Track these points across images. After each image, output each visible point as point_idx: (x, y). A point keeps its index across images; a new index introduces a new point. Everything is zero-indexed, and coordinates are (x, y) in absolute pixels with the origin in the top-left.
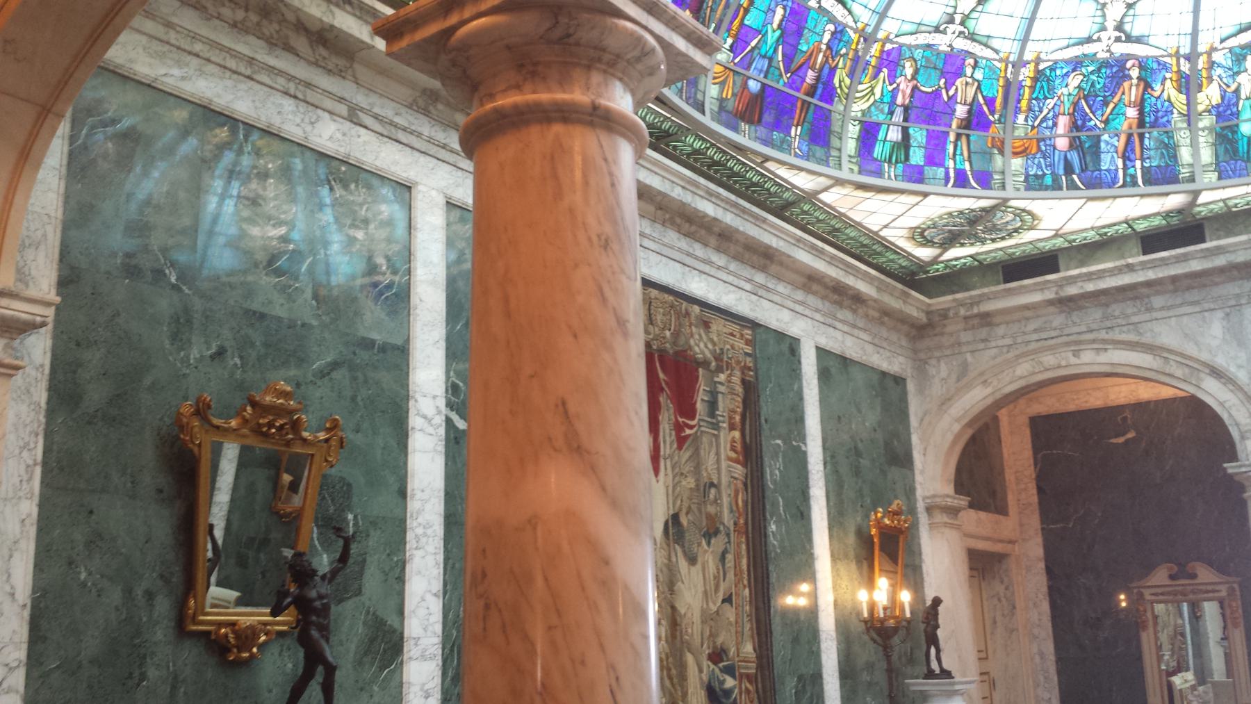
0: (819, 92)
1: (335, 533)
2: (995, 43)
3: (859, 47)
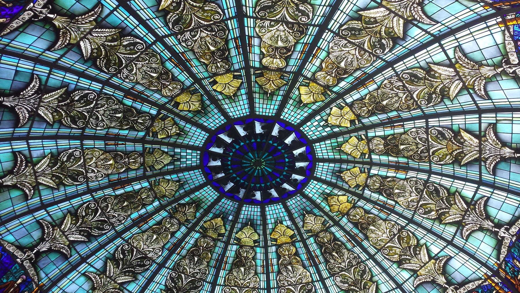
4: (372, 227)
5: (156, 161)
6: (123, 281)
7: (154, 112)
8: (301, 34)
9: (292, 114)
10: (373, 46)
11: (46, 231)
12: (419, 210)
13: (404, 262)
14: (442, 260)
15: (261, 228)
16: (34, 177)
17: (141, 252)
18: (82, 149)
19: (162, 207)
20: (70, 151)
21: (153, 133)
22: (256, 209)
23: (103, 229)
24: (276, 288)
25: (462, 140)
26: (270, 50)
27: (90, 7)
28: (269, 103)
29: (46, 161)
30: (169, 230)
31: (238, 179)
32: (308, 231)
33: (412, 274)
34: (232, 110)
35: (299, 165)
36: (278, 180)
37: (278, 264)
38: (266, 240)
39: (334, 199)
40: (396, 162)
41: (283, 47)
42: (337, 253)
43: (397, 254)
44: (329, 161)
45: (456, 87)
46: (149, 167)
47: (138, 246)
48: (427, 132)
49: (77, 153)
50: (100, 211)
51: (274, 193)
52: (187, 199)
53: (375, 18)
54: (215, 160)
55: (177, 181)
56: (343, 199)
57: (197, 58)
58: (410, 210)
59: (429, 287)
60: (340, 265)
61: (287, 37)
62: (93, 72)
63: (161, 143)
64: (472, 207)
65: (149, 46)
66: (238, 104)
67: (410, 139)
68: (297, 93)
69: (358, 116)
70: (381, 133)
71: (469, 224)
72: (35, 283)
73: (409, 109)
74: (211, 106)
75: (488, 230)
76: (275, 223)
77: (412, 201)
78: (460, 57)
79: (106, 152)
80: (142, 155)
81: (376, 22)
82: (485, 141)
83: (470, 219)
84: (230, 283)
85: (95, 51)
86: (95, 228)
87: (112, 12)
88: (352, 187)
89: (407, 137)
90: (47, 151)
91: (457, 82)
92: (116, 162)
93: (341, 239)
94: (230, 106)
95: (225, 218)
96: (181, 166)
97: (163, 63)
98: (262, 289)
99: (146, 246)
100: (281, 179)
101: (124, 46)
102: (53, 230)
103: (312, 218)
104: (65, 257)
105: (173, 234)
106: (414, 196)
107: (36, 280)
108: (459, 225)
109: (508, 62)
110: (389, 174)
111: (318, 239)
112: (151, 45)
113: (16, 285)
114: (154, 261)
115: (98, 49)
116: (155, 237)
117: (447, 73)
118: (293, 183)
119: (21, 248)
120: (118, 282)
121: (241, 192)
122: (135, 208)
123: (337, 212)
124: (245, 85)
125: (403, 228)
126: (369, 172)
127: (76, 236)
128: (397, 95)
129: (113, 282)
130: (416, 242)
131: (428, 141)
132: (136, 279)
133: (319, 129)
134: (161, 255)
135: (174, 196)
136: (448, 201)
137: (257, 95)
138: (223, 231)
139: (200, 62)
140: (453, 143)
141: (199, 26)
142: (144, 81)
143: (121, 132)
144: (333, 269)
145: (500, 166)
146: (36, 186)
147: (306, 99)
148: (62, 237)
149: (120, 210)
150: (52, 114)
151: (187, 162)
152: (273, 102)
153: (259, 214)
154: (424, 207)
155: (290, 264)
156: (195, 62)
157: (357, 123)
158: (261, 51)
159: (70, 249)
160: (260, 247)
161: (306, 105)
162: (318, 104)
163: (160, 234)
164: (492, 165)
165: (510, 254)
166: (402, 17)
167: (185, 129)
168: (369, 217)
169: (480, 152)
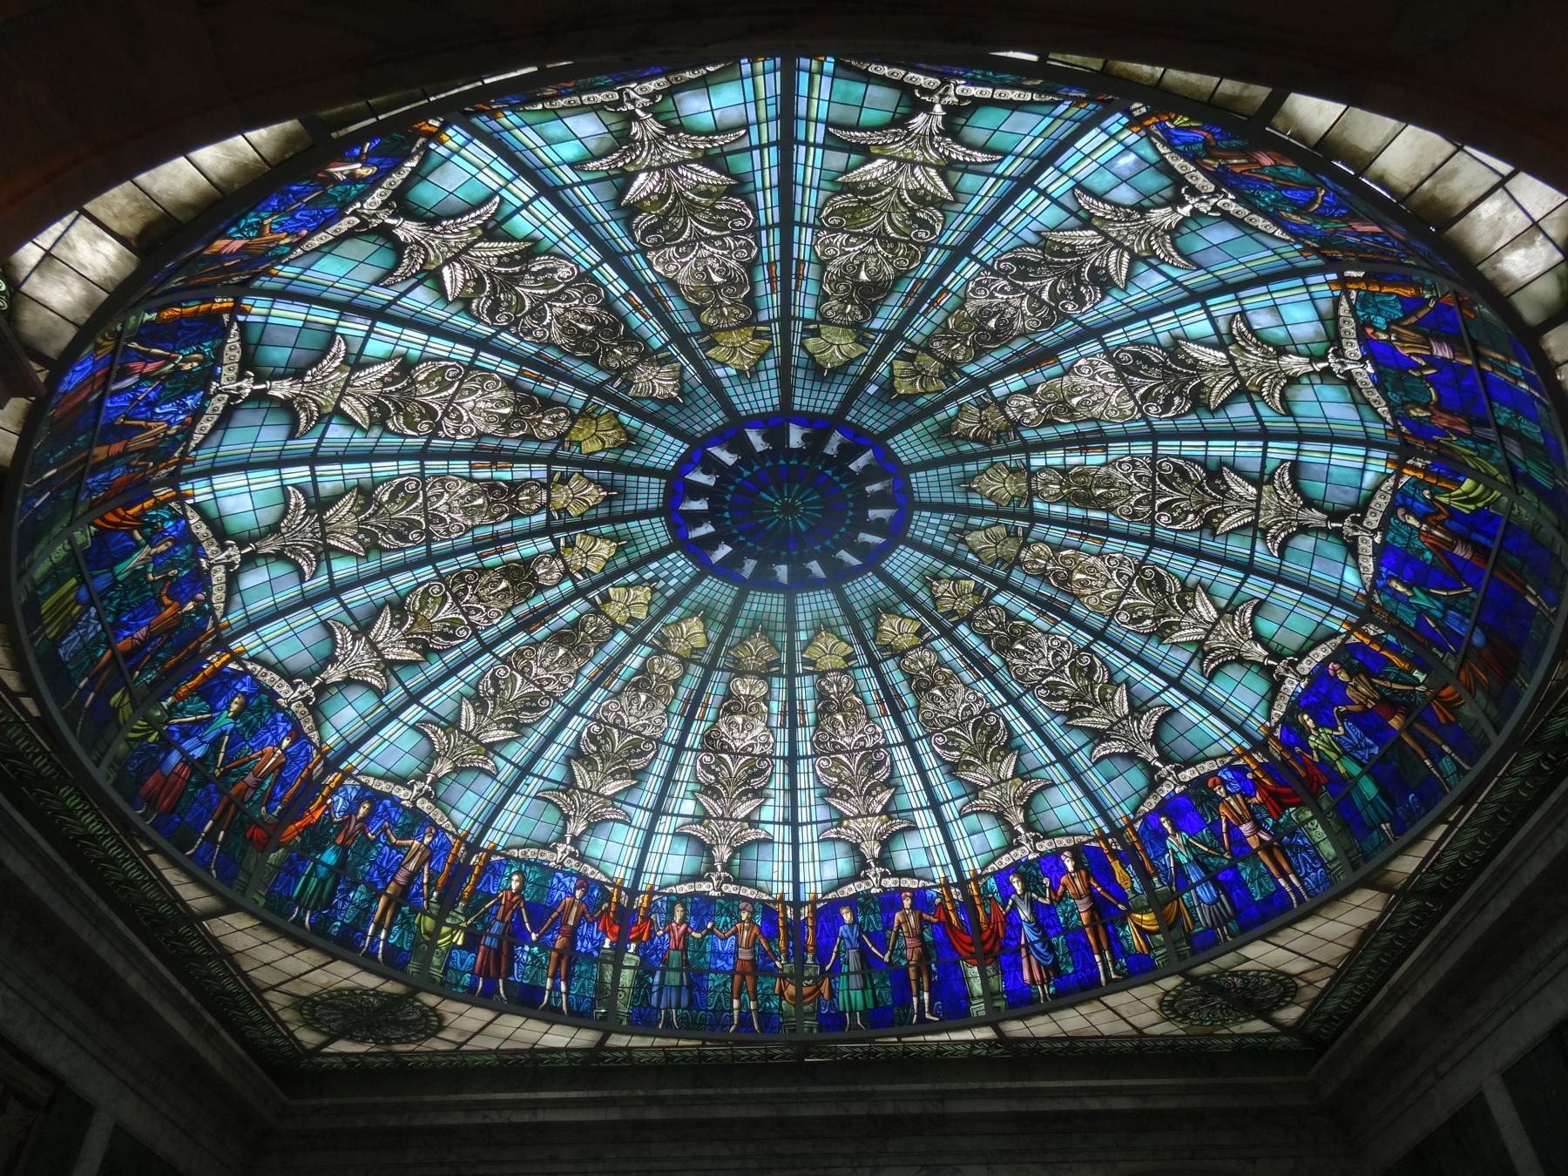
0: (1482, 539)
1: (404, 356)
2: (1325, 306)
3: (1420, 465)
4: (506, 411)
5: (997, 544)
6: (1211, 351)
7: (963, 630)
8: (709, 735)
9: (718, 595)
10: (606, 735)
11: (1283, 535)
12: (417, 486)
13: (396, 374)
14: (308, 423)
15: (794, 361)
16: (1218, 627)
17: (1126, 385)
18: (1111, 617)
19: (1029, 448)
20: (1130, 627)
21: (980, 595)
22: (805, 402)
23: (1178, 468)
24: (761, 228)
25: (412, 646)
26: (754, 709)
27: (974, 817)
28: (759, 615)
29: (1178, 637)
30: (1034, 403)
31: (837, 478)
32: (670, 360)
33: (362, 359)
34: (827, 605)
35: (700, 505)
36: (746, 473)
37: (753, 284)
38: (786, 333)
39: (611, 440)
40: (502, 551)
41: (736, 714)
42: (582, 331)
43: (421, 382)
44: (638, 515)
45: (468, 720)
46: (1016, 535)
47: (1126, 397)
48: (473, 625)
49: (1123, 617)
50: (1158, 502)
51: (755, 438)
52: (966, 448)
53: (615, 780)
54: (880, 520)
55: (974, 490)
56: (590, 446)
57: (865, 704)
58: (435, 476)
59: (301, 356)
60: (568, 305)
61: (730, 729)
62: (1020, 725)
63: (974, 570)
64: (320, 549)
65: (928, 736)
66: (816, 615)
67: (496, 607)
68: (711, 635)
69: (597, 611)
70: (548, 594)
71: (302, 520)
72: (1397, 481)
73: (519, 652)
74: (862, 616)
75: (262, 537)
76: (757, 372)
77: (440, 496)
78: (486, 763)
79: (1076, 597)
80: (1018, 562)
81: (612, 774)
82: (378, 665)
83: (308, 529)
84: (910, 249)
85: (999, 758)
86: (1191, 482)
87: (953, 800)
88: (575, 476)
89: (503, 606)
90: (1164, 649)
91: (471, 727)
92: (1071, 572)
93: (576, 363)
94: (830, 613)
95: (886, 391)
96: (952, 518)
97: (918, 706)
98: (807, 225)
99: (1107, 391)
100: (740, 474)
101: (959, 750)
102: (1270, 527)
103: (659, 391)
104: (1295, 468)
105: (1029, 390)
106: (441, 505)
107: (1391, 482)
108: (319, 504)
109: (427, 795)
110: (507, 525)
111: (640, 348)
112: (924, 737)
113: (1424, 527)
114: (1107, 351)
115: (993, 759)
116: (1075, 401)
117: (491, 734)
118: (712, 465)
119: (1352, 548)
120: (1223, 356)
121: (835, 447)
122: (1086, 475)
123: (600, 415)
124: (798, 646)
125: (434, 435)
126: (549, 514)
127: (1238, 489)
128: (547, 669)
129: (1238, 363)
130: (390, 425)
131: (462, 612)
132: (1175, 339)
133: (666, 573)
134: (1081, 357)
135: (993, 464)
136: (368, 533)
137: (780, 626)
138: (899, 365)
139: (862, 699)
140: (423, 634)
141: (850, 753)
142: (956, 686)
143: (1032, 618)
144: (586, 293)
145: (327, 645)
146: (1227, 611)
147: (694, 626)
148: (1267, 505)
149: (1117, 485)
150: (1112, 699)
151: (938, 522)
152: (752, 615)
153: (798, 392)
154: (409, 498)
155: (716, 288)
156: (870, 697)
157: (597, 598)
158: (768, 705)
159: (1272, 475)
160: (803, 319)
161: (694, 613)
162: (674, 618)
163: (1059, 402)
164: (339, 637)
165: (187, 537)
166: (582, 791)
167: (920, 585)
168: (522, 428)
169: (373, 645)
